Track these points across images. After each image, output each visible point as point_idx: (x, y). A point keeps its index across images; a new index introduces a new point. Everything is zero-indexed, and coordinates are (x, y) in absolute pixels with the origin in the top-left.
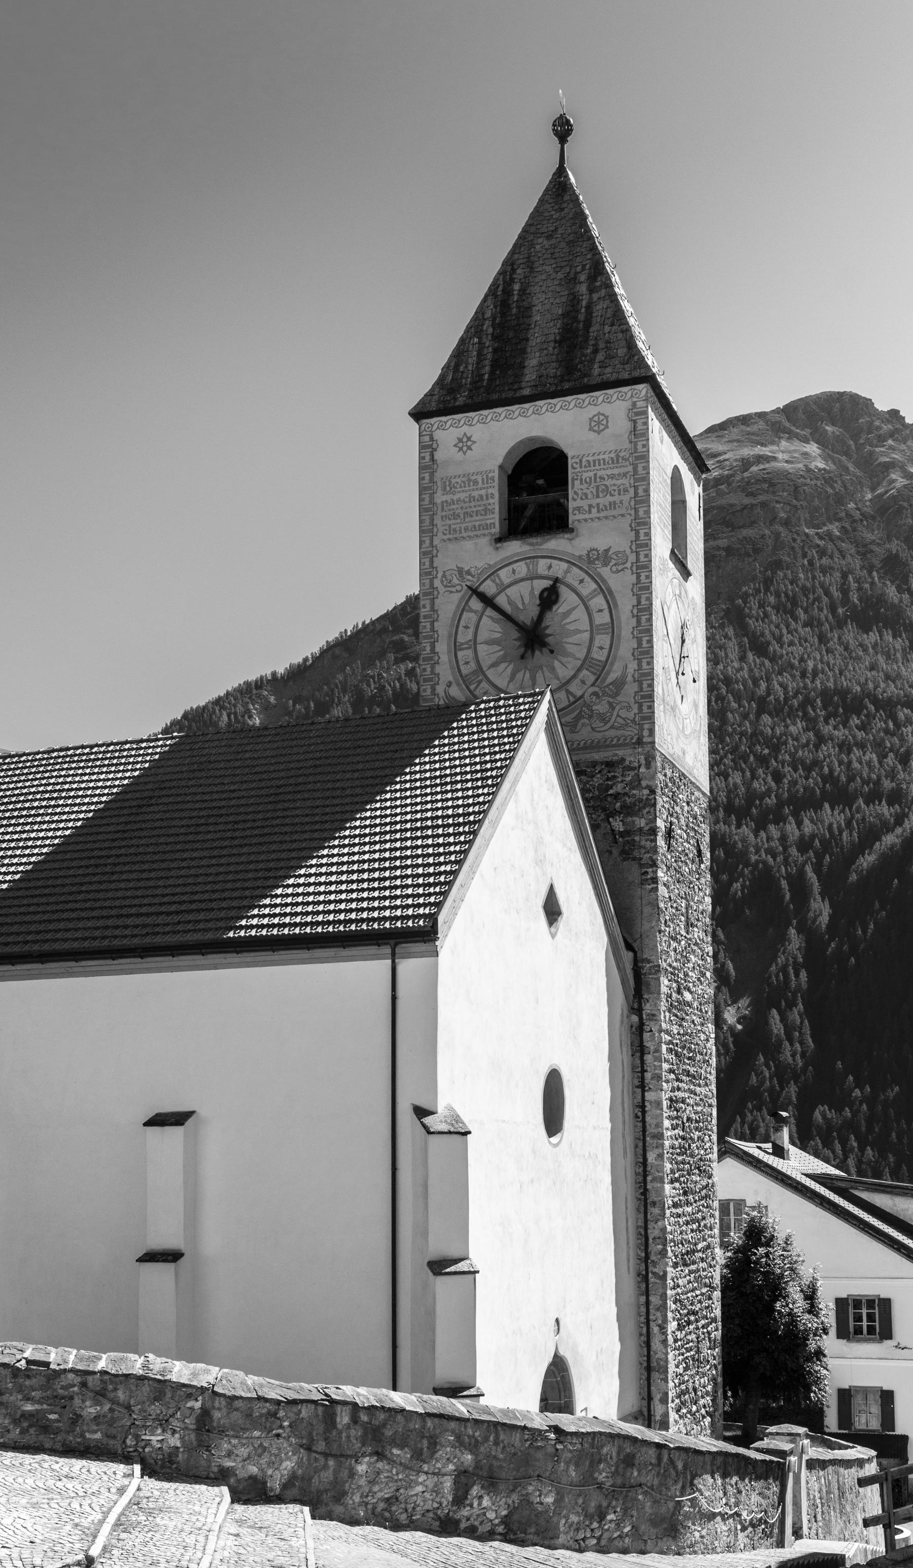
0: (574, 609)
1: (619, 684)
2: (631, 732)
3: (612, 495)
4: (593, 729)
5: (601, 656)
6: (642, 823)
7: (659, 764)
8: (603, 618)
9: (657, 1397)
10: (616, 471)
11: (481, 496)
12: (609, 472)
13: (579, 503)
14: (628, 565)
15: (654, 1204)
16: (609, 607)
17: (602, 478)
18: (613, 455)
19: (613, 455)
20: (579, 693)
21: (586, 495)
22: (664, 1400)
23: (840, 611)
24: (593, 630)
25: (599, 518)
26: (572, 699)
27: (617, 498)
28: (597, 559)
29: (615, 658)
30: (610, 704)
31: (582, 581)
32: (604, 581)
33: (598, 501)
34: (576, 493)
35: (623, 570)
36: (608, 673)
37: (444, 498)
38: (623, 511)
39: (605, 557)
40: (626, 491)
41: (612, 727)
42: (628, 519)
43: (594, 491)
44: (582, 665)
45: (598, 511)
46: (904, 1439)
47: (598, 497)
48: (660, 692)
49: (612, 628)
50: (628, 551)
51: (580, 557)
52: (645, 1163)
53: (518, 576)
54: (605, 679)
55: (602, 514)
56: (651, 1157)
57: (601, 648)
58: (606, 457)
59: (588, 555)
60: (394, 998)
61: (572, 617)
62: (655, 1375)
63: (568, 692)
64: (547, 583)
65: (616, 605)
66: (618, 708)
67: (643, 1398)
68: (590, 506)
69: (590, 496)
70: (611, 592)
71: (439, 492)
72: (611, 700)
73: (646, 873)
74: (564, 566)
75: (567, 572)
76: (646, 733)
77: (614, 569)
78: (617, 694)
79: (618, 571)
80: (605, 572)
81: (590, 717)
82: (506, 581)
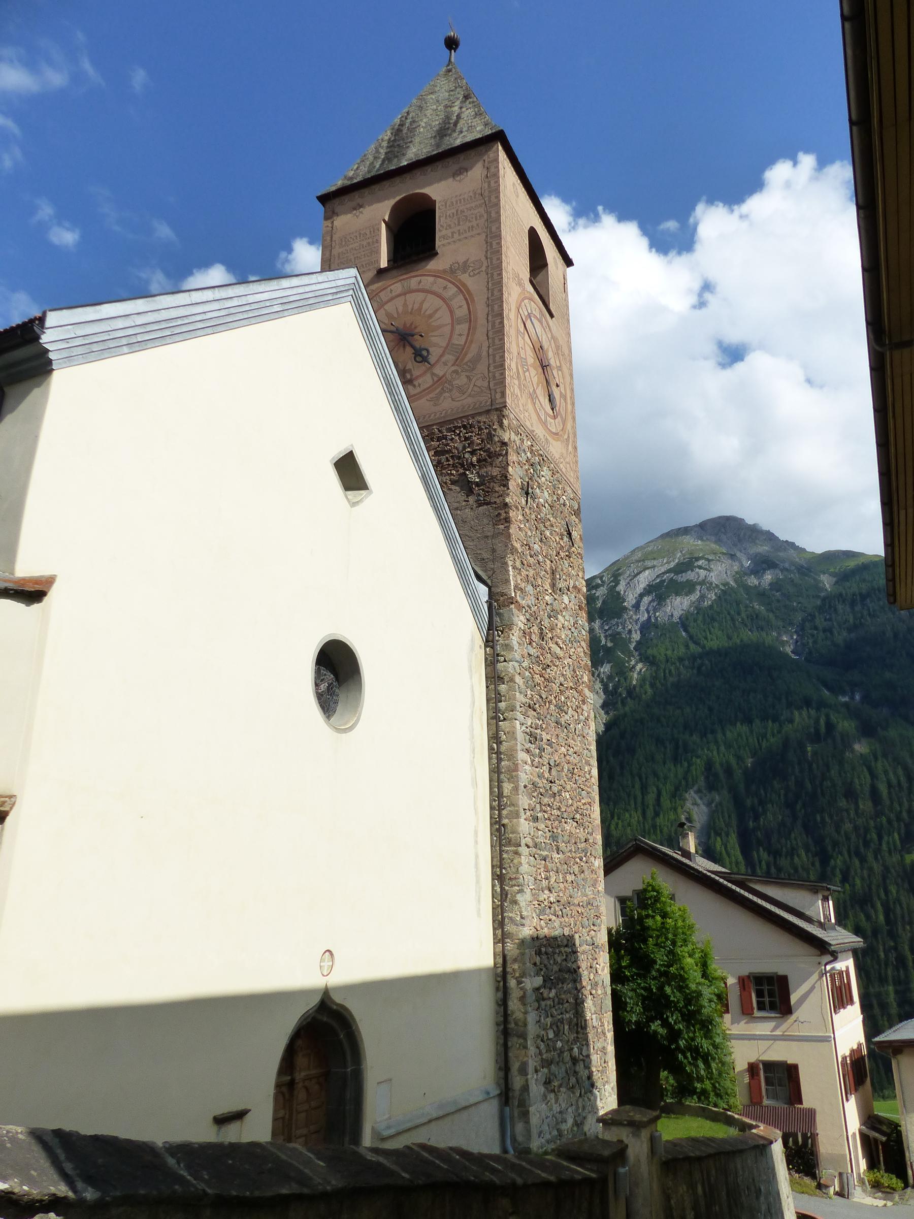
0: (437, 310)
1: (477, 359)
2: (485, 399)
3: (470, 221)
4: (453, 400)
5: (460, 341)
6: (495, 472)
7: (593, 727)
8: (462, 312)
9: (515, 1066)
10: (473, 205)
11: (369, 243)
12: (468, 206)
13: (444, 232)
14: (484, 268)
15: (509, 842)
16: (468, 303)
17: (462, 211)
18: (471, 194)
19: (471, 194)
20: (441, 374)
21: (450, 226)
22: (523, 1071)
23: (835, 818)
24: (455, 321)
25: (460, 240)
26: (436, 379)
27: (474, 223)
28: (458, 269)
29: (472, 342)
30: (468, 377)
31: (445, 288)
32: (464, 285)
33: (458, 228)
34: (442, 226)
35: (479, 273)
36: (466, 355)
37: (340, 250)
38: (478, 232)
39: (465, 267)
40: (481, 216)
41: (470, 395)
42: (484, 236)
43: (456, 222)
44: (444, 352)
45: (459, 234)
46: (811, 1113)
47: (459, 225)
48: (513, 366)
49: (470, 319)
50: (483, 259)
51: (445, 271)
52: (500, 795)
53: (394, 294)
54: (463, 359)
55: (462, 236)
56: (507, 788)
57: (460, 335)
58: (466, 196)
59: (451, 268)
60: (417, 1127)
61: (437, 316)
62: (514, 1041)
63: (433, 374)
64: (432, 359)
65: (473, 301)
66: (474, 380)
67: (500, 1069)
68: (453, 233)
69: (453, 225)
70: (468, 291)
71: (337, 247)
72: (467, 374)
73: (499, 514)
74: (431, 279)
75: (455, 296)
76: (498, 396)
77: (472, 274)
78: (473, 369)
79: (475, 275)
80: (464, 278)
81: (451, 390)
82: (385, 299)
